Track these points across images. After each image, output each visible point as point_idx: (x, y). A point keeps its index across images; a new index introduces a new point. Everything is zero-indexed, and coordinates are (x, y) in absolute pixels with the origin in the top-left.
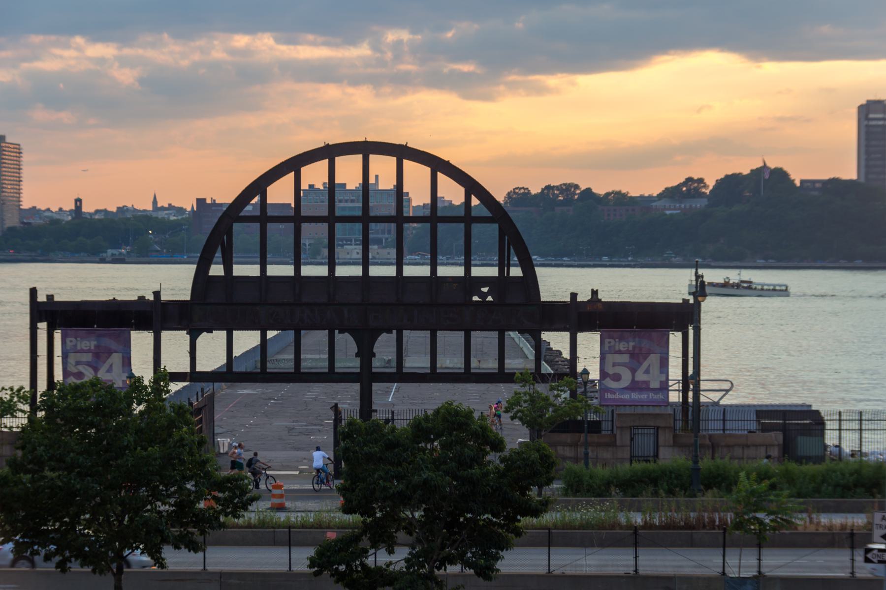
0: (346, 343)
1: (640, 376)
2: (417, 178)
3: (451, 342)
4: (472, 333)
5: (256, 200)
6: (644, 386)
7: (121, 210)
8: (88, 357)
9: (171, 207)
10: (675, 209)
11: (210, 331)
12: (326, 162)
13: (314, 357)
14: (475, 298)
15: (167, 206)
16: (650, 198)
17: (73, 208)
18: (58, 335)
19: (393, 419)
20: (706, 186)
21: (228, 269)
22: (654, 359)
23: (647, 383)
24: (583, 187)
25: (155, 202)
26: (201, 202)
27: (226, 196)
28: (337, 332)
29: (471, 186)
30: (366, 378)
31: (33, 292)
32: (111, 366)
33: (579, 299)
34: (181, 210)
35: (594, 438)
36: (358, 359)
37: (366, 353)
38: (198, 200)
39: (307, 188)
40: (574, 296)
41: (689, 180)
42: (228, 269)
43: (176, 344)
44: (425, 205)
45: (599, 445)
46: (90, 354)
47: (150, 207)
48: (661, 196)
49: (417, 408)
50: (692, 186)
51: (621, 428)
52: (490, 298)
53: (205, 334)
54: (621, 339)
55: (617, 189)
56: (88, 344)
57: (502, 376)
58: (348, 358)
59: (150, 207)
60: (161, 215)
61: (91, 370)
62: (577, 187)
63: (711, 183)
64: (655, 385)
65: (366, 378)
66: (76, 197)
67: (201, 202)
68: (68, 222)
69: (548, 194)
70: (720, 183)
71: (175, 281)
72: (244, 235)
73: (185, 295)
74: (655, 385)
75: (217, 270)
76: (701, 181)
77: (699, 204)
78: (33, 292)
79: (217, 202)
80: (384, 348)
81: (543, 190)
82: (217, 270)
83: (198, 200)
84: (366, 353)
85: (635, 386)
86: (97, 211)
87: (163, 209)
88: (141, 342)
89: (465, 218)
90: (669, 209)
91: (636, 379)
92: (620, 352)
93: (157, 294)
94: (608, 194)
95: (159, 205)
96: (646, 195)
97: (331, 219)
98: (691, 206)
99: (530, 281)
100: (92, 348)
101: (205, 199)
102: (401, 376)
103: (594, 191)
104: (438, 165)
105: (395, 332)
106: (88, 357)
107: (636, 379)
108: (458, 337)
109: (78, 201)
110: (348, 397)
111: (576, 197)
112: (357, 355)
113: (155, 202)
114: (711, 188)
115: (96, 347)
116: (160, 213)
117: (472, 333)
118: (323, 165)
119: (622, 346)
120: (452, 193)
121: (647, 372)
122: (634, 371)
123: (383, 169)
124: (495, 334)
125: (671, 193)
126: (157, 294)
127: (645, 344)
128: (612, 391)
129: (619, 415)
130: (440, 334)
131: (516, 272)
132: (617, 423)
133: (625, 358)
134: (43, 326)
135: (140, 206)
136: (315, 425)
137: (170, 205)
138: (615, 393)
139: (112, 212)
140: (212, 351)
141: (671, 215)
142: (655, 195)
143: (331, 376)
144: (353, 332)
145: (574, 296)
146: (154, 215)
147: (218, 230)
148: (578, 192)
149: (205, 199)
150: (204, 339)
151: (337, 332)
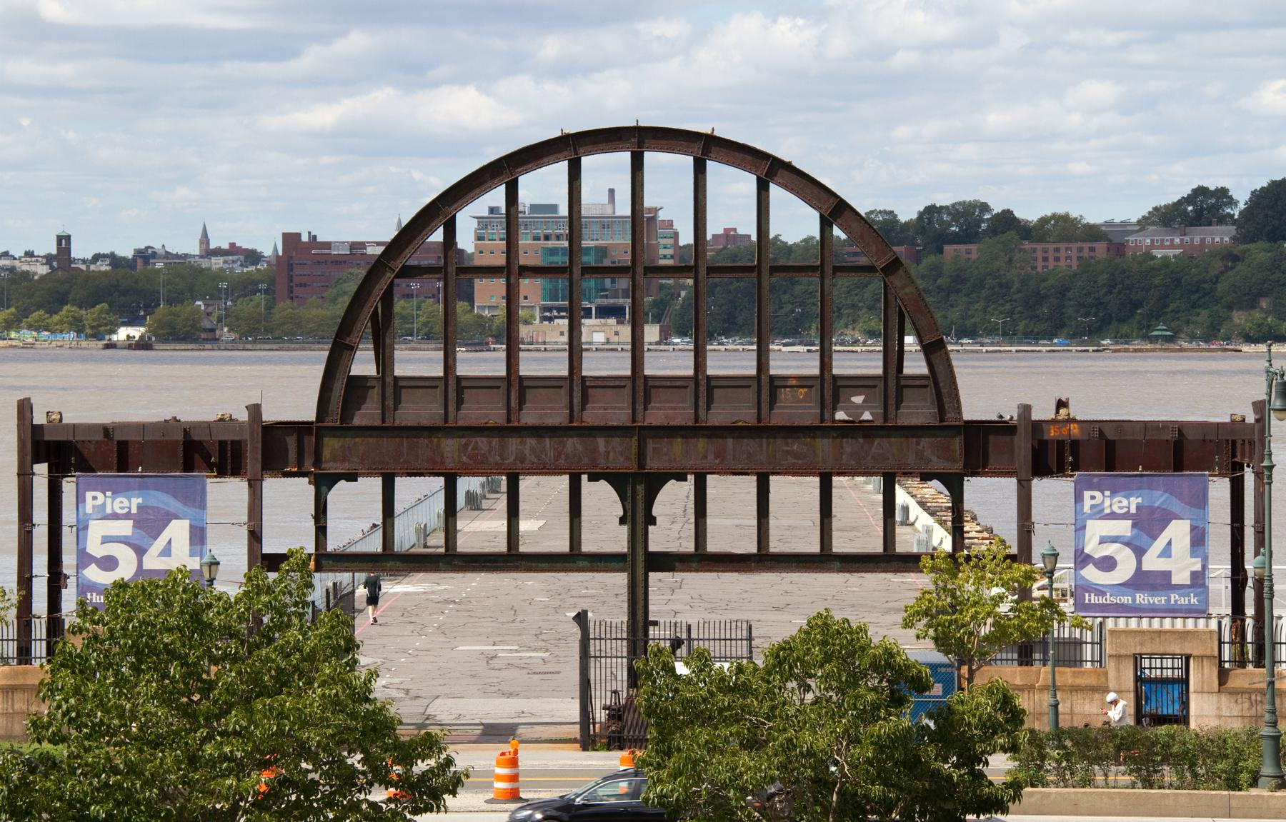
0: (601, 500)
1: (1152, 562)
2: (732, 192)
3: (794, 495)
4: (835, 479)
5: (438, 236)
6: (1159, 581)
7: (145, 255)
8: (1123, 528)
9: (234, 250)
10: (1172, 246)
11: (352, 477)
12: (563, 166)
13: (542, 527)
14: (840, 415)
15: (226, 246)
16: (1124, 228)
17: (53, 250)
18: (68, 487)
19: (690, 639)
20: (1232, 202)
21: (384, 360)
22: (1179, 531)
23: (1167, 575)
24: (997, 209)
25: (205, 239)
26: (291, 240)
27: (378, 229)
28: (584, 478)
29: (834, 209)
30: (641, 563)
31: (24, 408)
32: (1169, 543)
33: (1035, 416)
34: (253, 257)
35: (1066, 675)
36: (625, 529)
37: (638, 516)
38: (287, 237)
39: (486, 214)
40: (1026, 409)
41: (1200, 192)
42: (384, 360)
43: (288, 499)
44: (807, 240)
45: (1076, 689)
46: (130, 523)
47: (193, 248)
48: (1144, 223)
49: (723, 618)
50: (1204, 206)
51: (1118, 657)
52: (867, 416)
53: (673, 481)
54: (116, 492)
55: (1061, 210)
56: (126, 503)
57: (892, 560)
58: (604, 521)
59: (193, 248)
60: (217, 263)
61: (1128, 552)
62: (985, 207)
63: (1242, 197)
64: (1181, 577)
65: (641, 563)
66: (60, 232)
67: (291, 240)
68: (43, 278)
69: (930, 222)
70: (1259, 198)
71: (286, 386)
72: (417, 302)
73: (306, 411)
74: (1181, 577)
75: (363, 364)
76: (1222, 193)
77: (1220, 236)
78: (24, 408)
79: (319, 239)
80: (674, 499)
81: (921, 214)
82: (363, 364)
83: (287, 237)
84: (638, 516)
85: (1142, 580)
86: (97, 258)
87: (218, 252)
88: (226, 494)
89: (819, 262)
90: (1162, 247)
91: (1145, 567)
92: (1113, 516)
93: (255, 410)
94: (1044, 221)
95: (212, 246)
96: (1117, 220)
97: (512, 271)
98: (1202, 240)
99: (941, 384)
100: (134, 510)
101: (299, 235)
102: (703, 559)
103: (1018, 214)
104: (770, 170)
105: (691, 478)
106: (125, 528)
107: (1145, 567)
108: (871, 487)
109: (64, 241)
110: (605, 595)
111: (984, 226)
112: (622, 521)
113: (205, 239)
114: (1242, 206)
115: (139, 507)
116: (214, 260)
117: (835, 479)
118: (560, 170)
119: (120, 504)
120: (795, 222)
121: (1166, 552)
122: (1140, 552)
123: (668, 174)
124: (750, 483)
125: (1168, 217)
126: (255, 410)
127: (1160, 498)
128: (1099, 591)
129: (1112, 632)
130: (401, 483)
131: (915, 365)
132: (1108, 649)
133: (125, 528)
134: (41, 469)
135: (176, 247)
136: (535, 650)
137: (232, 245)
138: (1104, 594)
139: (124, 258)
140: (354, 512)
141: (1165, 258)
142: (1134, 220)
143: (574, 559)
144: (618, 481)
145: (1026, 409)
146: (205, 264)
147: (365, 294)
148: (987, 216)
149: (299, 235)
150: (340, 493)
151: (584, 478)
